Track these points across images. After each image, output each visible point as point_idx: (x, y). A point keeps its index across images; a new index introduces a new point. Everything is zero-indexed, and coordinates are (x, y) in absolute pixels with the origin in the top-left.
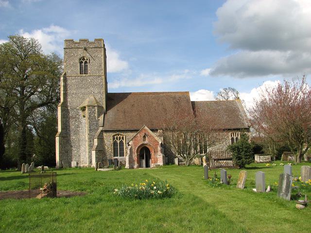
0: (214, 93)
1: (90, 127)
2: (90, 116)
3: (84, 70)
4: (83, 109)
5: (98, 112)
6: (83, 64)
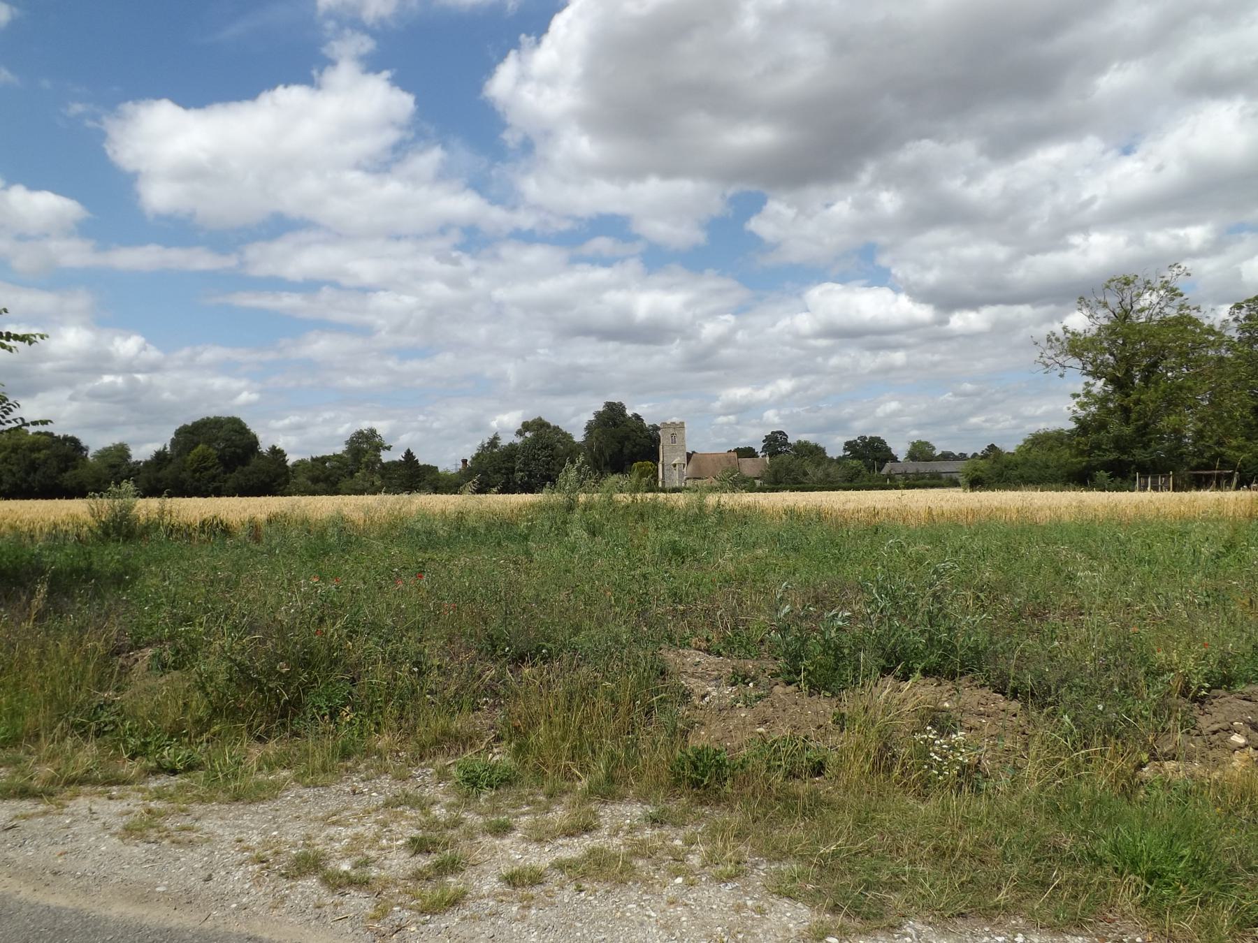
4: (675, 465)
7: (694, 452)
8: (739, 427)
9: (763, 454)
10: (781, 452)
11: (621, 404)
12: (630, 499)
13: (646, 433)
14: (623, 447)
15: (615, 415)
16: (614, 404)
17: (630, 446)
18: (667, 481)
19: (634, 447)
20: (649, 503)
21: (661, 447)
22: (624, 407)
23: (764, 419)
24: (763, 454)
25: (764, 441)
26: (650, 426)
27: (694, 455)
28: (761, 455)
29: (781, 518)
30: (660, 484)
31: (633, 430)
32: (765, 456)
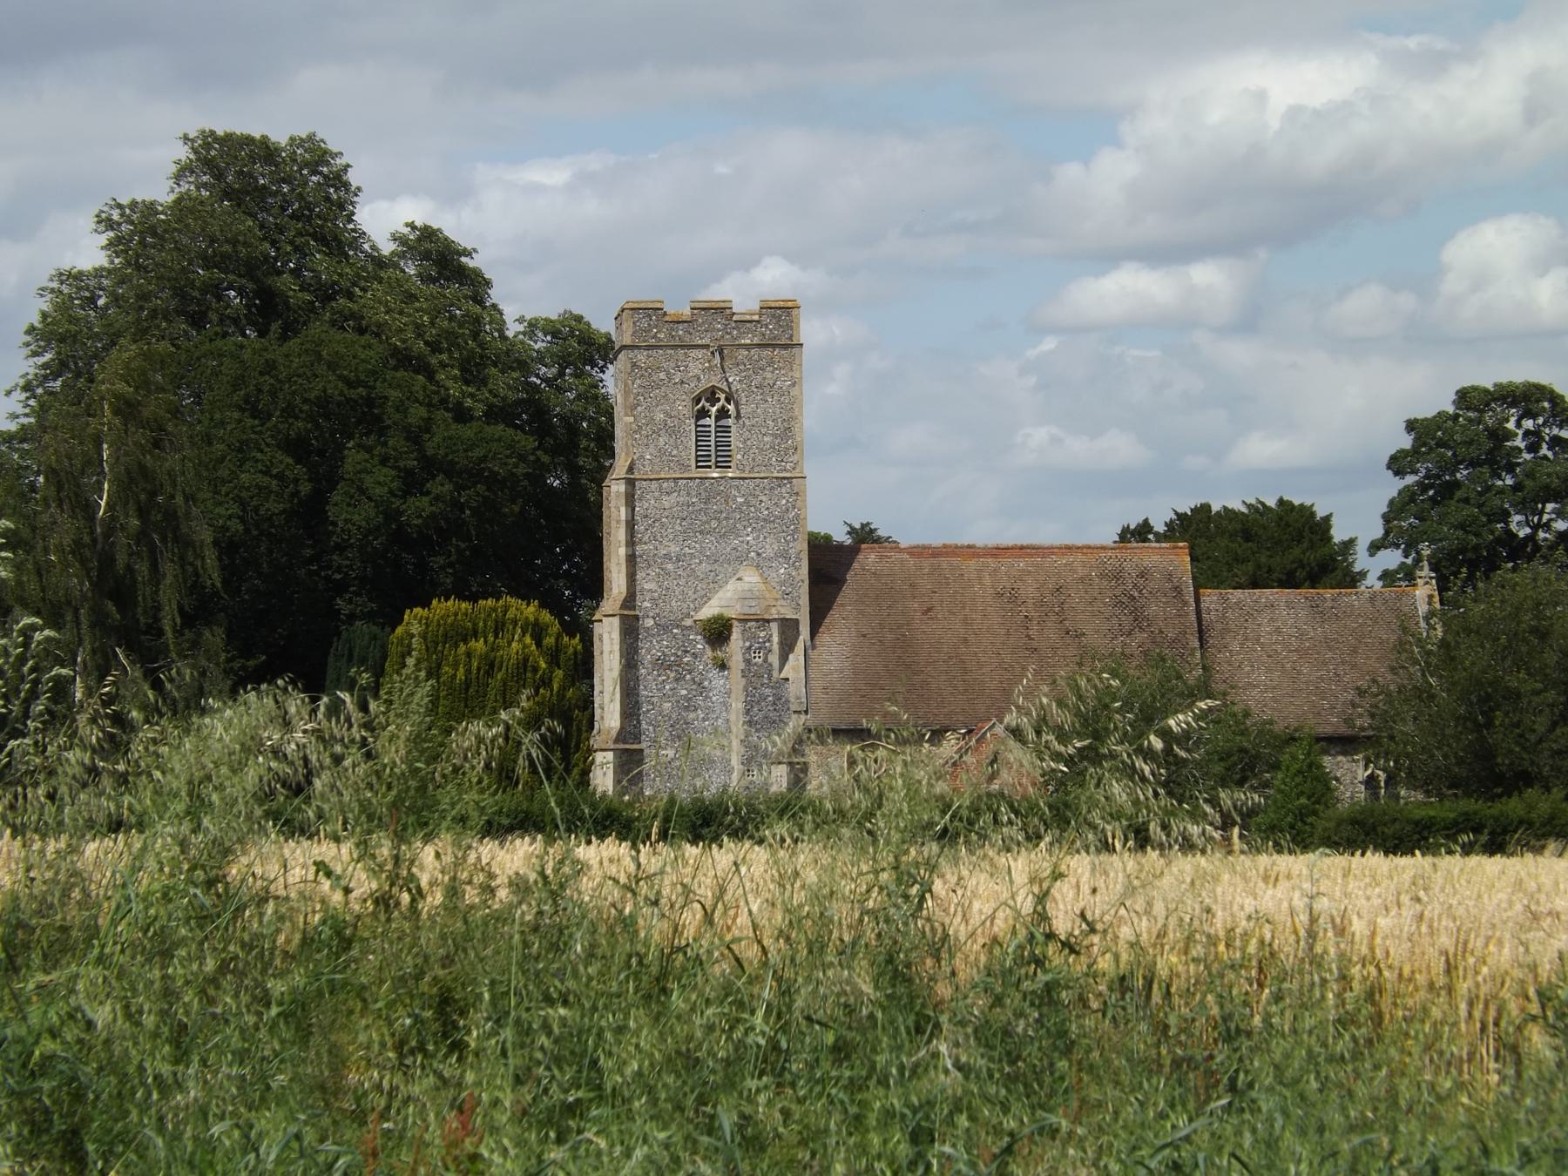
0: (604, 793)
1: (747, 712)
2: (748, 662)
3: (714, 453)
4: (718, 632)
5: (781, 643)
6: (710, 421)
7: (865, 535)
8: (1240, 354)
9: (1392, 558)
10: (1521, 550)
11: (316, 155)
12: (365, 884)
13: (503, 384)
14: (326, 481)
15: (271, 235)
16: (264, 151)
17: (382, 480)
18: (661, 753)
19: (412, 484)
20: (504, 917)
21: (615, 489)
22: (338, 180)
23: (1452, 285)
24: (1392, 558)
25: (1398, 464)
26: (533, 326)
27: (868, 558)
28: (1373, 566)
29: (1510, 1051)
30: (604, 779)
31: (404, 359)
32: (1408, 574)
